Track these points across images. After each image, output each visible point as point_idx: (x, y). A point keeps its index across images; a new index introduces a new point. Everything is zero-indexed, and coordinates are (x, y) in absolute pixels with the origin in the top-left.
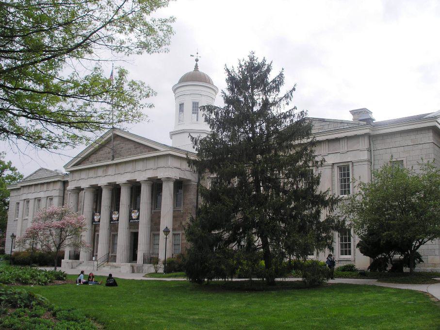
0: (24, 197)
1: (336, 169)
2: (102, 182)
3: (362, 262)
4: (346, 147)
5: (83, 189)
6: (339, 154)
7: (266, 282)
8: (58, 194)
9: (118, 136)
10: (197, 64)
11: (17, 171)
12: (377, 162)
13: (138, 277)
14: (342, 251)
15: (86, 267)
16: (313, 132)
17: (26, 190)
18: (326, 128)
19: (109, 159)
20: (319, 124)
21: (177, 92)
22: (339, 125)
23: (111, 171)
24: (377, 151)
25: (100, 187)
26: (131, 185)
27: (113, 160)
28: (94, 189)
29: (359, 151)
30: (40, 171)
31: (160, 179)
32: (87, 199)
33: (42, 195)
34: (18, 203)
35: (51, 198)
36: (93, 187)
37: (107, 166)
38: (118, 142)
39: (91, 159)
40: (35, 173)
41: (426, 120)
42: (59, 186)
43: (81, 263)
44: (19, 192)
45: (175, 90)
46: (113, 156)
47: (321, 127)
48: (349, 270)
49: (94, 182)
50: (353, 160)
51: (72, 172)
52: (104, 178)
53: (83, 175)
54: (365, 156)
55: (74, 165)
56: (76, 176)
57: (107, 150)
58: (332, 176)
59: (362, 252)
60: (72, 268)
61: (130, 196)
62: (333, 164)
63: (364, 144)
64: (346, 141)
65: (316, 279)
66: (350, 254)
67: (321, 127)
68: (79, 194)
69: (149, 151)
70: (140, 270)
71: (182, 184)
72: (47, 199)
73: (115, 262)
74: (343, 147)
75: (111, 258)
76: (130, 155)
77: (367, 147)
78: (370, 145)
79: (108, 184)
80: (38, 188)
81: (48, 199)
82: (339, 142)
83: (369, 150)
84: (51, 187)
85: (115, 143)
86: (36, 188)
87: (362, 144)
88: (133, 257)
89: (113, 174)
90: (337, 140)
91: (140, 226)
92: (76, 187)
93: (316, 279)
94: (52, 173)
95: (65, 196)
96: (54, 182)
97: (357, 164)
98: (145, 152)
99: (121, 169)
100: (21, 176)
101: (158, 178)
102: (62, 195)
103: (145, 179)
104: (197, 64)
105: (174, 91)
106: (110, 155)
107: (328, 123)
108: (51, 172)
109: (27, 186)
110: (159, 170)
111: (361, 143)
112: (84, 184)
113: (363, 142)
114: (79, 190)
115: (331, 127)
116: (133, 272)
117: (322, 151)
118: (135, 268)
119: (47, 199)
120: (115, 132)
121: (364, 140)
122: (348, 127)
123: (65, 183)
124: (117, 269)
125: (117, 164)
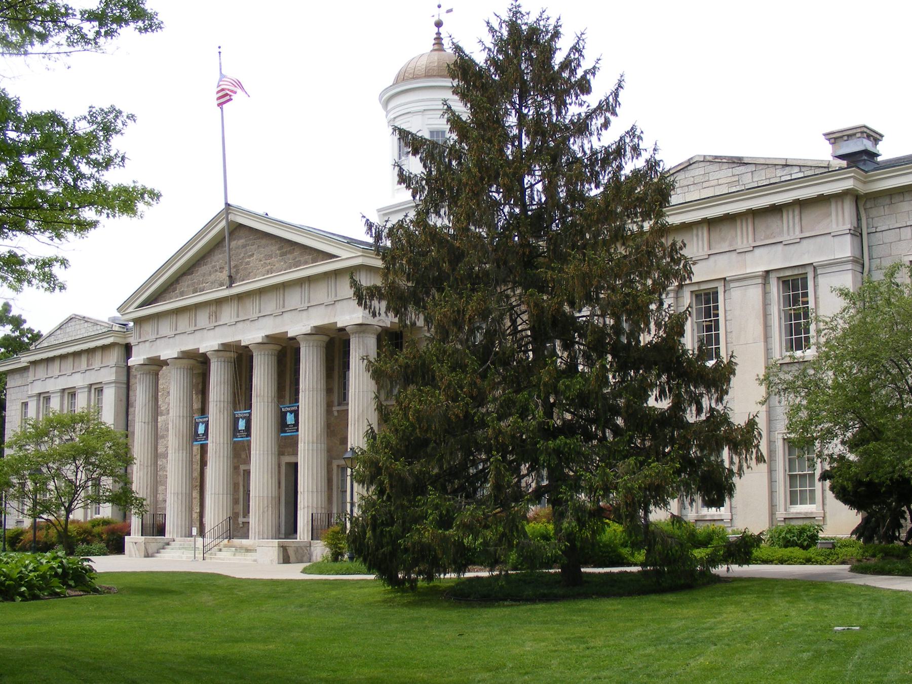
0: (38, 388)
1: (774, 288)
2: (208, 343)
3: (841, 521)
4: (798, 228)
5: (165, 363)
6: (780, 247)
7: (564, 577)
8: (113, 378)
9: (241, 226)
10: (438, 34)
11: (25, 326)
12: (876, 262)
13: (294, 572)
14: (793, 494)
15: (178, 557)
16: (674, 199)
17: (41, 372)
18: (749, 180)
19: (221, 285)
20: (729, 172)
21: (392, 105)
22: (779, 172)
23: (228, 314)
24: (877, 234)
25: (247, 347)
26: (278, 348)
27: (230, 286)
28: (192, 361)
29: (829, 237)
30: (72, 323)
31: (342, 330)
32: (174, 387)
33: (78, 381)
34: (25, 404)
35: (97, 389)
36: (187, 355)
37: (219, 302)
38: (241, 242)
39: (180, 287)
40: (60, 327)
41: (746, 194)
42: (114, 357)
43: (168, 544)
44: (25, 375)
45: (387, 100)
46: (230, 277)
47: (736, 178)
48: (801, 540)
49: (189, 344)
50: (815, 259)
51: (139, 321)
52: (211, 333)
53: (165, 328)
54: (845, 249)
55: (142, 305)
56: (149, 330)
57: (219, 259)
58: (766, 304)
59: (837, 497)
60: (147, 555)
61: (275, 376)
62: (767, 272)
63: (842, 219)
64: (797, 212)
65: (680, 570)
66: (812, 501)
67: (736, 178)
68: (157, 374)
69: (314, 261)
70: (302, 555)
71: (402, 338)
72: (90, 391)
73: (247, 537)
74: (789, 227)
75: (236, 528)
76: (195, 291)
77: (849, 226)
78: (859, 219)
79: (180, 356)
80: (68, 365)
81: (93, 391)
82: (779, 217)
83: (857, 233)
84: (97, 361)
85: (233, 244)
86: (77, 361)
87: (742, 234)
88: (288, 527)
89: (233, 320)
90: (775, 210)
91: (301, 446)
92: (267, 336)
93: (680, 570)
94: (99, 327)
95: (132, 381)
96: (104, 348)
97: (737, 284)
98: (306, 263)
99: (251, 308)
100: (36, 337)
101: (289, 335)
102: (124, 379)
103: (307, 329)
104: (438, 34)
105: (386, 103)
106: (224, 276)
107: (752, 168)
108: (96, 323)
109: (42, 361)
110: (338, 305)
111: (834, 214)
112: (168, 352)
113: (744, 229)
114: (156, 365)
115: (762, 177)
116: (286, 560)
117: (834, 226)
118: (291, 552)
119: (90, 391)
120: (231, 217)
121: (843, 209)
122: (801, 175)
123: (128, 349)
124: (250, 557)
125: (240, 297)
